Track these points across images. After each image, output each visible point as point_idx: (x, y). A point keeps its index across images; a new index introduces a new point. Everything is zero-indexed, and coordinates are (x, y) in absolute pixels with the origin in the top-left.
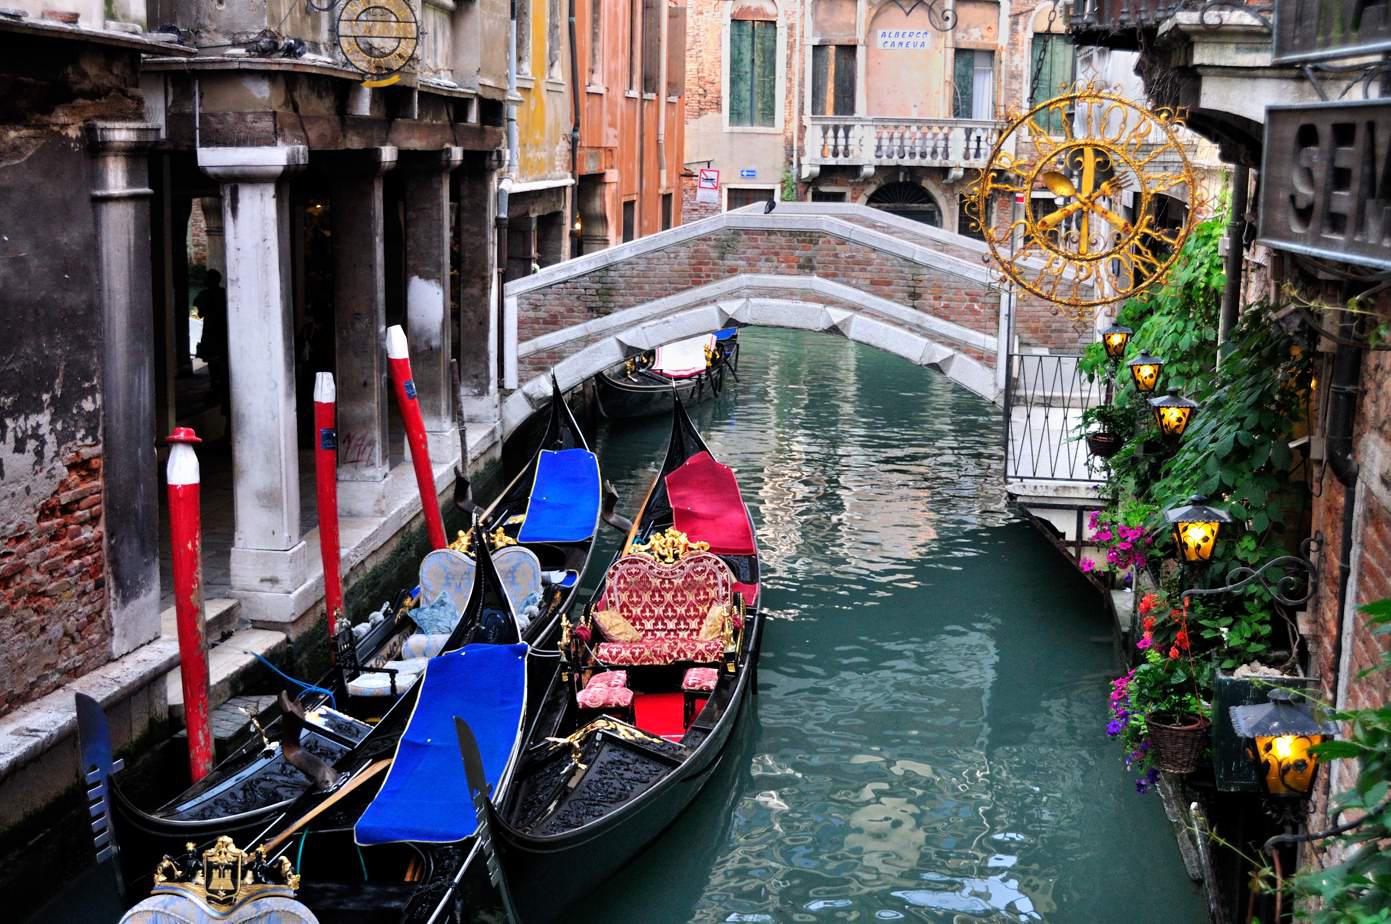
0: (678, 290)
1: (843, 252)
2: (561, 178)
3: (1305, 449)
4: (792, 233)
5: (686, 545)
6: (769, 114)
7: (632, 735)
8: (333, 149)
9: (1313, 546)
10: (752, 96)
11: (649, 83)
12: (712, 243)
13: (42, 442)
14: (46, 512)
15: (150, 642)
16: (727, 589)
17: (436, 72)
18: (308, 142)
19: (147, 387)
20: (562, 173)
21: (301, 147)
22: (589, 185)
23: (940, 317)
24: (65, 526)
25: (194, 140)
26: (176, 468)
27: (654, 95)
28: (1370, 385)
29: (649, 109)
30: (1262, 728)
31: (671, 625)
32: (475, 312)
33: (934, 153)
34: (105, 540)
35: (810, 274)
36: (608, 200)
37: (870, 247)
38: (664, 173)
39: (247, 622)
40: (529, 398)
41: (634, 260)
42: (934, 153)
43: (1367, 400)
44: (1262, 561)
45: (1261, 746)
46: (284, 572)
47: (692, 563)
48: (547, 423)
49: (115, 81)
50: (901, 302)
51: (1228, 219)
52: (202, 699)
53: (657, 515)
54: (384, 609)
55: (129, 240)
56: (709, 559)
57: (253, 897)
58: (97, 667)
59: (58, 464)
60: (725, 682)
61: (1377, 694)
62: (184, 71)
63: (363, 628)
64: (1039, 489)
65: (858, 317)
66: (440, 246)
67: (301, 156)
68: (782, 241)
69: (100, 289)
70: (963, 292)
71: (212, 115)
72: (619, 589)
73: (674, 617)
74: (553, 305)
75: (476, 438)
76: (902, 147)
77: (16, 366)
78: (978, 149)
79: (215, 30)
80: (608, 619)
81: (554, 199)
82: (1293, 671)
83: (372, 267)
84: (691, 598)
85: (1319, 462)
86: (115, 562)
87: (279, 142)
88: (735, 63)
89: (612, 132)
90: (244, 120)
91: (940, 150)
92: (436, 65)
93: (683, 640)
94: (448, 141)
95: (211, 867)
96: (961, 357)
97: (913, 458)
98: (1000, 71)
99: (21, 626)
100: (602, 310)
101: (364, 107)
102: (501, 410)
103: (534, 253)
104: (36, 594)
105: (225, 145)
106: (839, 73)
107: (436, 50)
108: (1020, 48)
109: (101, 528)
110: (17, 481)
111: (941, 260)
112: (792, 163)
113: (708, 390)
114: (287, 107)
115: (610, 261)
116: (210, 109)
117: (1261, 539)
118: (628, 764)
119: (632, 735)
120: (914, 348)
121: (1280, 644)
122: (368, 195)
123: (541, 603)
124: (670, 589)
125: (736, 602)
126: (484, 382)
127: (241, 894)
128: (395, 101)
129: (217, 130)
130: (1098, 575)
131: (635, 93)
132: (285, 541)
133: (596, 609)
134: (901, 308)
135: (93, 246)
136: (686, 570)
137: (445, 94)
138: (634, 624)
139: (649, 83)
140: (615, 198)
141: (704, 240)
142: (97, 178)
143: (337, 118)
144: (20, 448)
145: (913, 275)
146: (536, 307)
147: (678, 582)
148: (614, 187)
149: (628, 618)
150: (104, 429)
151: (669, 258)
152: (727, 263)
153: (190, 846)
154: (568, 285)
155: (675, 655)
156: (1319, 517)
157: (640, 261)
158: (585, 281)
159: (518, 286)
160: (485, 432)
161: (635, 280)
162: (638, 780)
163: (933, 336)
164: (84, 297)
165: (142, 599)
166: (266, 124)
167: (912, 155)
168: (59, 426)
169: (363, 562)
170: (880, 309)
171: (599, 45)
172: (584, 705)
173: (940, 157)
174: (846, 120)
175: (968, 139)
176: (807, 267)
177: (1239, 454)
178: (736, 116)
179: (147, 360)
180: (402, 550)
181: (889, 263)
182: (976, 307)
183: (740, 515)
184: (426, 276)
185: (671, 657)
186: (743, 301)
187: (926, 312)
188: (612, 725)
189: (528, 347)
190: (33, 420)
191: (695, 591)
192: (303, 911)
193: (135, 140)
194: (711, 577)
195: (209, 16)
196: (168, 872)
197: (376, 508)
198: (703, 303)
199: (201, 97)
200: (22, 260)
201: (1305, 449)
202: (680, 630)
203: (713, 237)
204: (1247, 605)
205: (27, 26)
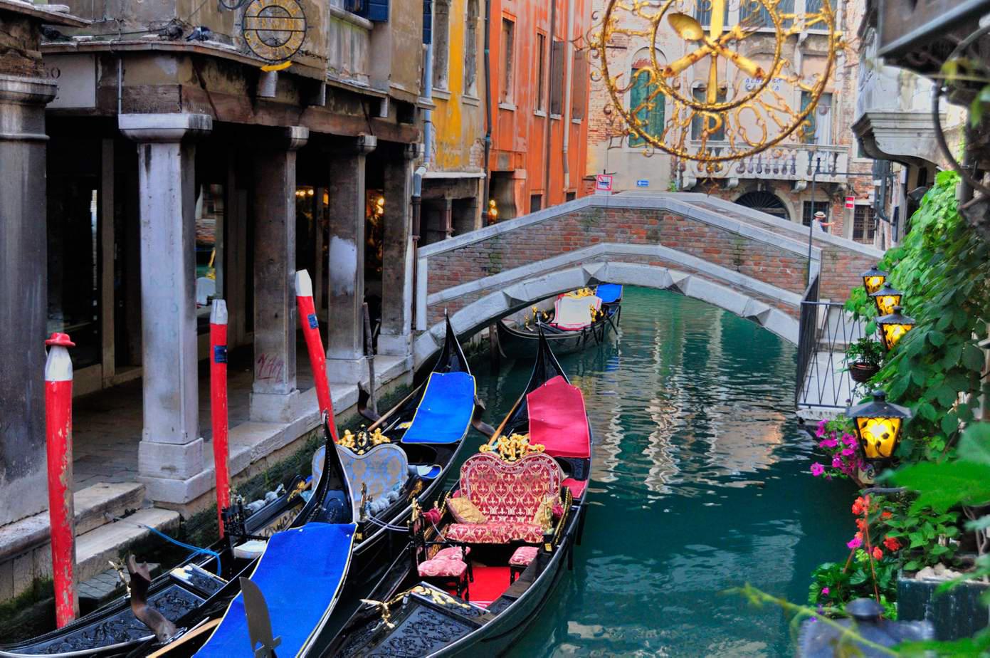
0: (552, 255)
1: (683, 227)
2: (475, 172)
5: (526, 447)
7: (444, 599)
8: (243, 122)
11: (555, 106)
12: (579, 218)
15: (36, 514)
16: (557, 484)
17: (353, 75)
19: (39, 299)
20: (476, 168)
21: (205, 116)
23: (759, 279)
25: (117, 109)
26: (51, 367)
27: (560, 116)
29: (555, 132)
31: (511, 511)
32: (393, 269)
33: (784, 169)
35: (656, 244)
36: (517, 192)
37: (703, 222)
38: (567, 176)
39: (150, 502)
40: (435, 337)
41: (518, 231)
42: (784, 169)
46: (180, 463)
47: (530, 461)
48: (449, 353)
49: (13, 43)
50: (729, 266)
52: (68, 564)
53: (518, 424)
54: (278, 490)
55: (23, 175)
56: (544, 458)
60: (541, 559)
62: (108, 52)
63: (259, 504)
64: (824, 415)
65: (694, 279)
66: (356, 213)
67: (204, 123)
68: (634, 217)
70: (778, 259)
71: (131, 88)
72: (471, 481)
73: (513, 505)
75: (384, 368)
76: (759, 164)
78: (818, 167)
79: (136, 20)
80: (458, 504)
81: (468, 187)
84: (528, 490)
87: (184, 110)
89: (521, 141)
90: (156, 92)
91: (789, 167)
92: (352, 69)
93: (520, 524)
94: (364, 131)
96: (775, 311)
97: (635, 363)
98: (836, 109)
100: (493, 270)
101: (270, 90)
102: (413, 347)
103: (448, 226)
105: (141, 112)
107: (352, 59)
108: (852, 91)
111: (761, 234)
112: (676, 176)
113: (592, 341)
114: (195, 83)
115: (500, 231)
116: (129, 82)
118: (434, 625)
119: (444, 599)
120: (741, 305)
122: (281, 165)
123: (402, 490)
124: (511, 482)
125: (563, 495)
126: (400, 324)
128: (304, 88)
129: (135, 100)
131: (542, 113)
132: (182, 436)
133: (451, 496)
134: (728, 271)
136: (525, 467)
137: (356, 91)
138: (481, 510)
139: (555, 106)
140: (524, 189)
141: (573, 216)
143: (247, 98)
145: (738, 245)
146: (442, 267)
148: (522, 183)
149: (476, 504)
151: (545, 229)
152: (592, 234)
154: (467, 250)
155: (510, 536)
157: (523, 232)
158: (480, 247)
160: (396, 363)
161: (519, 246)
162: (440, 639)
165: (29, 478)
166: (174, 95)
167: (768, 171)
169: (264, 458)
170: (711, 272)
171: (512, 74)
172: (423, 573)
173: (789, 173)
174: (717, 144)
175: (811, 160)
176: (653, 238)
177: (937, 353)
179: (40, 277)
180: (307, 451)
181: (719, 236)
182: (788, 272)
183: (583, 427)
184: (344, 237)
185: (507, 537)
186: (603, 264)
187: (748, 275)
188: (428, 591)
189: (435, 298)
191: (532, 484)
193: (29, 91)
194: (545, 473)
195: (132, 9)
197: (283, 416)
198: (571, 265)
199: (124, 73)
202: (518, 515)
203: (580, 213)
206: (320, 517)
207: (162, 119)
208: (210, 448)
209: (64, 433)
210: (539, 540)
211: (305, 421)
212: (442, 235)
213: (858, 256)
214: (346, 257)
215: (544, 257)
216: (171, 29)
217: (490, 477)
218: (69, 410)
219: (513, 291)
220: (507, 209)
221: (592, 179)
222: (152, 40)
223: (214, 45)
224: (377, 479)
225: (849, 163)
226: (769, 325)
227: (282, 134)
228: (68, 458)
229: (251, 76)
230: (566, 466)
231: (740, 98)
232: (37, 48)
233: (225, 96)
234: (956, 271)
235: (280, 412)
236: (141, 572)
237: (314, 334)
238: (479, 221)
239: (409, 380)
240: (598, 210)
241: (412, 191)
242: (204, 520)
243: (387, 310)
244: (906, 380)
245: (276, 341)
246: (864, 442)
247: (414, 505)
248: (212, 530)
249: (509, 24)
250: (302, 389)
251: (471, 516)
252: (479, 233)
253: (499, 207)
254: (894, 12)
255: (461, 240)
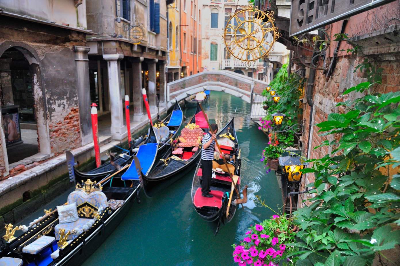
0: (196, 84)
1: (224, 78)
3: (302, 101)
4: (216, 75)
6: (216, 59)
9: (303, 121)
10: (214, 56)
11: (195, 52)
13: (65, 105)
14: (66, 118)
17: (153, 45)
18: (124, 54)
22: (183, 69)
24: (71, 121)
28: (317, 83)
29: (195, 57)
30: (287, 163)
31: (192, 140)
34: (80, 125)
40: (171, 103)
43: (316, 87)
44: (293, 125)
45: (286, 168)
46: (120, 131)
48: (175, 106)
51: (288, 64)
57: (94, 191)
58: (79, 147)
59: (68, 110)
61: (317, 154)
63: (137, 140)
65: (227, 89)
69: (77, 78)
74: (175, 87)
75: (161, 110)
77: (58, 91)
80: (181, 139)
82: (299, 148)
83: (139, 78)
85: (305, 104)
86: (82, 128)
88: (211, 51)
89: (188, 59)
95: (86, 185)
99: (60, 140)
101: (135, 49)
103: (173, 78)
104: (64, 134)
106: (228, 53)
109: (79, 122)
110: (59, 113)
113: (204, 103)
116: (105, 48)
117: (293, 121)
120: (236, 94)
121: (296, 142)
122: (138, 66)
127: (92, 190)
128: (142, 48)
130: (266, 132)
135: (75, 69)
142: (76, 56)
144: (59, 106)
146: (172, 87)
147: (193, 132)
150: (79, 104)
153: (82, 181)
156: (305, 116)
159: (170, 84)
163: (240, 92)
164: (74, 79)
166: (115, 50)
168: (68, 102)
176: (218, 80)
177: (289, 102)
178: (211, 59)
184: (151, 81)
189: (171, 94)
190: (62, 101)
192: (103, 194)
196: (79, 186)
198: (200, 86)
200: (59, 71)
201: (302, 101)
204: (289, 134)
205: (56, 25)
206: (150, 142)
207: (113, 56)
208: (126, 128)
209: (96, 125)
210: (198, 146)
211: (145, 122)
212: (172, 81)
213: (261, 84)
214: (152, 86)
215: (194, 85)
216: (114, 35)
217: (187, 133)
218: (97, 120)
219: (189, 92)
220: (185, 75)
221: (203, 68)
222: (109, 38)
223: (123, 39)
224: (162, 134)
225: (258, 64)
226: (243, 98)
227: (138, 59)
228: (97, 130)
229: (132, 46)
230: (204, 130)
231: (255, 47)
232: (85, 40)
233: (126, 50)
234: (293, 85)
235: (140, 120)
236: (113, 155)
237: (147, 102)
238: (180, 77)
239: (166, 112)
240: (206, 74)
241: (165, 71)
242: (126, 143)
243: (161, 97)
244: (283, 108)
245: (138, 104)
246: (275, 121)
247: (171, 139)
248: (127, 146)
249: (185, 34)
250: (144, 114)
251: (184, 141)
252: (180, 80)
253: (184, 74)
254: (294, 27)
255: (176, 82)
